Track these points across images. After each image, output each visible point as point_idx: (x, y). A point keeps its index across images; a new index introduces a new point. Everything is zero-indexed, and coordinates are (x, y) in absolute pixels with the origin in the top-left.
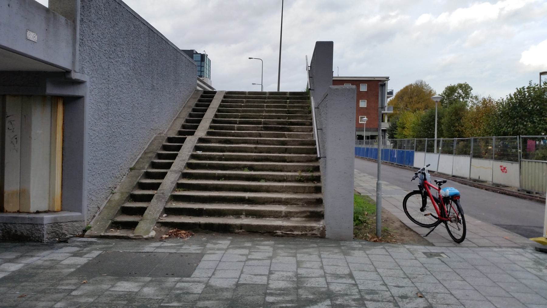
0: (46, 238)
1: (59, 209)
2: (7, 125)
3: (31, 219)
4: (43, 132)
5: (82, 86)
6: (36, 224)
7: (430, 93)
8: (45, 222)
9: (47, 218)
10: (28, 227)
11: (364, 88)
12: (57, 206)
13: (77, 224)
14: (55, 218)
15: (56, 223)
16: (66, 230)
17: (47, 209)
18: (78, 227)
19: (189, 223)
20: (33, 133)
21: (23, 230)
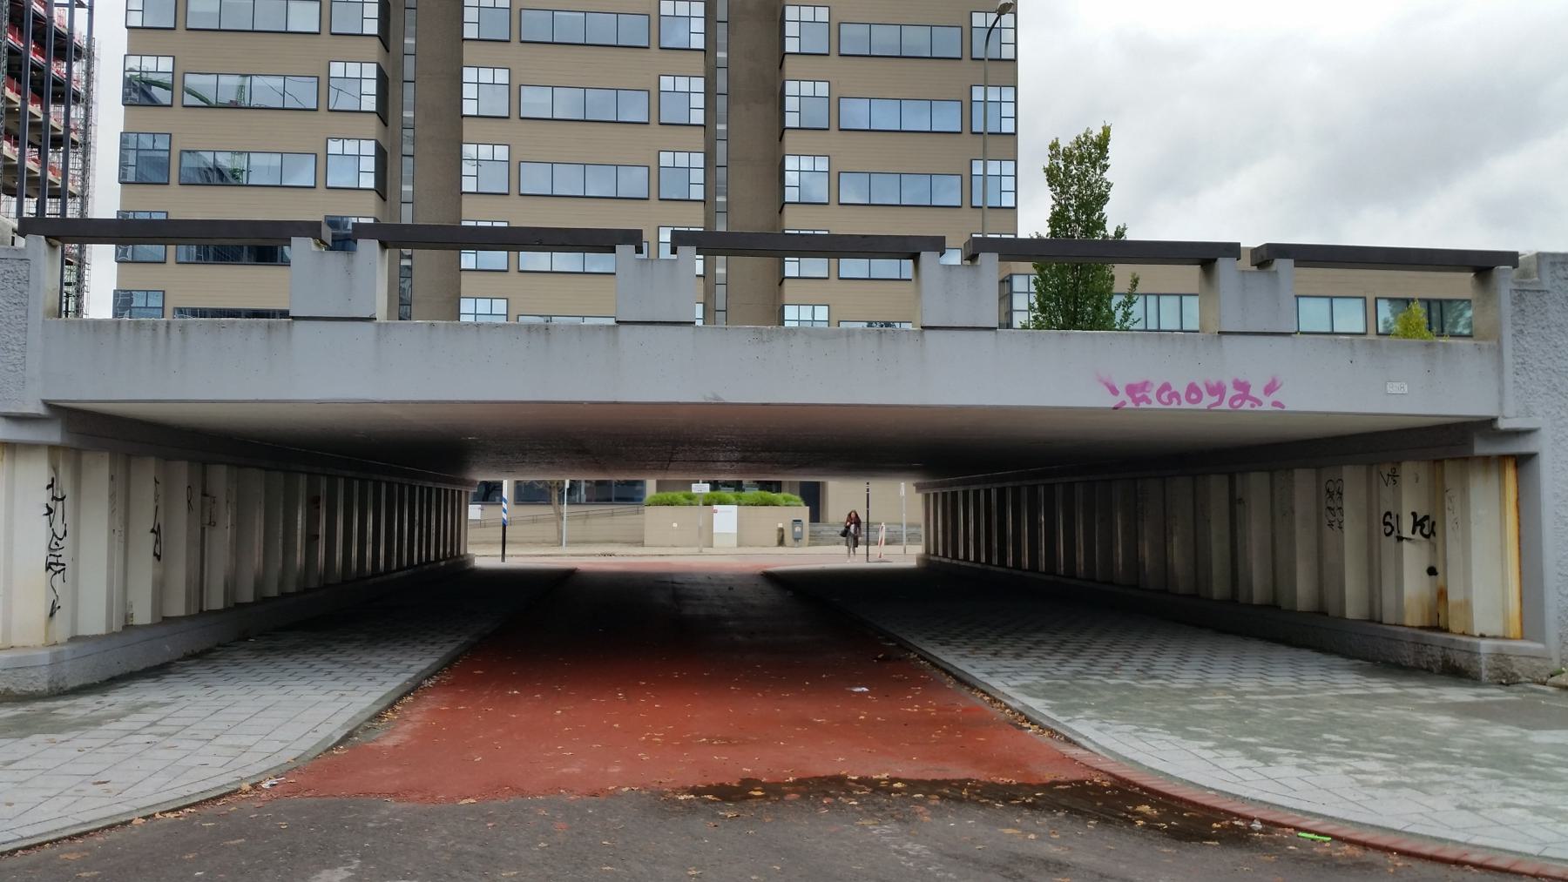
0: (1485, 674)
1: (1518, 634)
2: (1448, 504)
3: (1468, 644)
4: (1485, 513)
5: (1532, 437)
6: (1472, 652)
7: (1040, 240)
8: (1483, 650)
9: (1485, 646)
10: (1466, 655)
11: (1419, 311)
12: (1515, 628)
13: (1537, 663)
14: (1499, 648)
15: (1499, 656)
16: (1517, 667)
17: (1500, 633)
18: (1539, 668)
19: (564, 579)
20: (1473, 514)
21: (1460, 659)
